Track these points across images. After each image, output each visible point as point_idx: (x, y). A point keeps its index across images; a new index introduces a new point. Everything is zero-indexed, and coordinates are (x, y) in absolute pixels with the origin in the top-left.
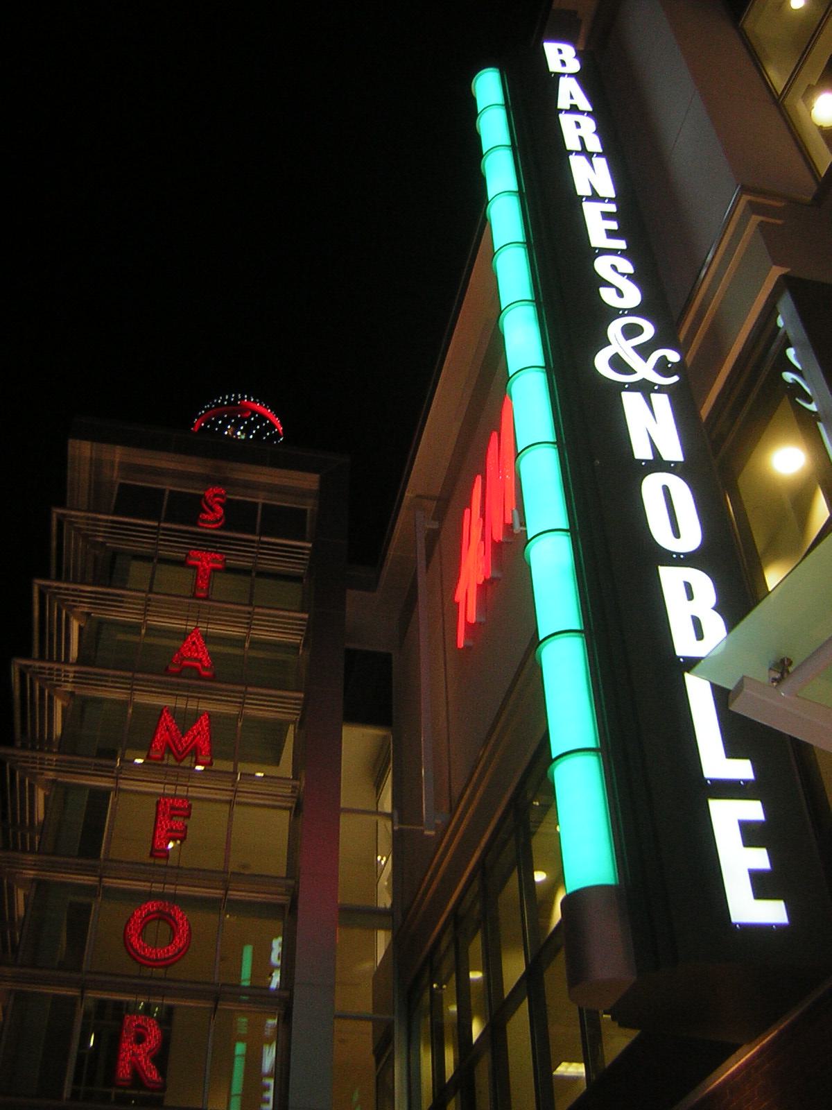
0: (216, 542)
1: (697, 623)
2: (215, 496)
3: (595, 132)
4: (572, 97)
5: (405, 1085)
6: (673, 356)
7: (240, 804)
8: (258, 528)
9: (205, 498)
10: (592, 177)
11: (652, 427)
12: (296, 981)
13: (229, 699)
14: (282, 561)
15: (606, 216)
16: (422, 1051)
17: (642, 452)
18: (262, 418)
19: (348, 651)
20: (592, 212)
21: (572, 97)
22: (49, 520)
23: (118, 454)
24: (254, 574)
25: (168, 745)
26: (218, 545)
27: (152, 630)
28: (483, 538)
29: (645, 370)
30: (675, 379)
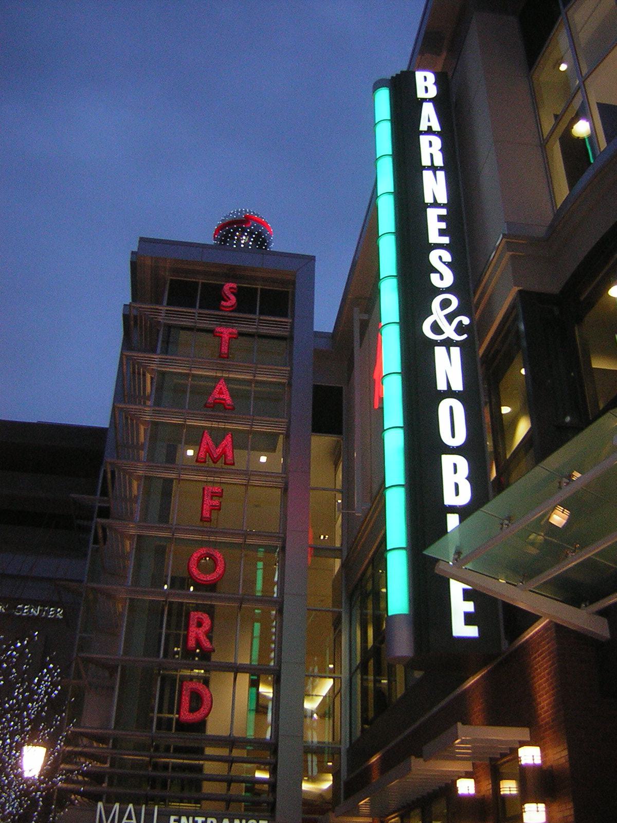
0: (232, 320)
1: (457, 486)
3: (440, 150)
4: (429, 121)
5: (348, 643)
6: (466, 321)
10: (435, 187)
11: (449, 369)
15: (441, 218)
17: (441, 386)
20: (432, 215)
21: (429, 121)
29: (449, 331)
30: (465, 336)
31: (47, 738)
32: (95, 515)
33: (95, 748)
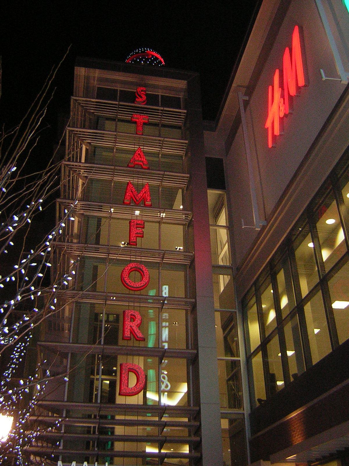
2: (142, 91)
5: (243, 336)
7: (164, 223)
8: (160, 103)
9: (137, 93)
12: (199, 345)
13: (99, 254)
14: (171, 119)
16: (249, 324)
18: (156, 59)
19: (206, 157)
22: (70, 101)
23: (97, 73)
24: (160, 125)
25: (132, 197)
26: (145, 112)
27: (120, 151)
28: (282, 96)
31: (21, 397)
32: (45, 257)
33: (34, 446)
